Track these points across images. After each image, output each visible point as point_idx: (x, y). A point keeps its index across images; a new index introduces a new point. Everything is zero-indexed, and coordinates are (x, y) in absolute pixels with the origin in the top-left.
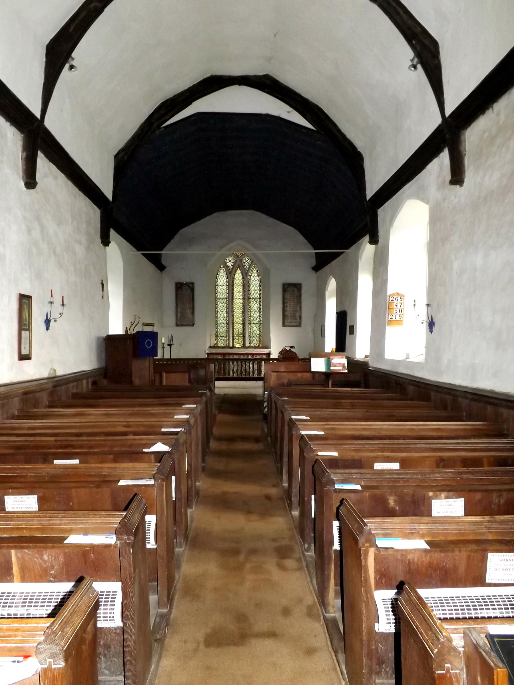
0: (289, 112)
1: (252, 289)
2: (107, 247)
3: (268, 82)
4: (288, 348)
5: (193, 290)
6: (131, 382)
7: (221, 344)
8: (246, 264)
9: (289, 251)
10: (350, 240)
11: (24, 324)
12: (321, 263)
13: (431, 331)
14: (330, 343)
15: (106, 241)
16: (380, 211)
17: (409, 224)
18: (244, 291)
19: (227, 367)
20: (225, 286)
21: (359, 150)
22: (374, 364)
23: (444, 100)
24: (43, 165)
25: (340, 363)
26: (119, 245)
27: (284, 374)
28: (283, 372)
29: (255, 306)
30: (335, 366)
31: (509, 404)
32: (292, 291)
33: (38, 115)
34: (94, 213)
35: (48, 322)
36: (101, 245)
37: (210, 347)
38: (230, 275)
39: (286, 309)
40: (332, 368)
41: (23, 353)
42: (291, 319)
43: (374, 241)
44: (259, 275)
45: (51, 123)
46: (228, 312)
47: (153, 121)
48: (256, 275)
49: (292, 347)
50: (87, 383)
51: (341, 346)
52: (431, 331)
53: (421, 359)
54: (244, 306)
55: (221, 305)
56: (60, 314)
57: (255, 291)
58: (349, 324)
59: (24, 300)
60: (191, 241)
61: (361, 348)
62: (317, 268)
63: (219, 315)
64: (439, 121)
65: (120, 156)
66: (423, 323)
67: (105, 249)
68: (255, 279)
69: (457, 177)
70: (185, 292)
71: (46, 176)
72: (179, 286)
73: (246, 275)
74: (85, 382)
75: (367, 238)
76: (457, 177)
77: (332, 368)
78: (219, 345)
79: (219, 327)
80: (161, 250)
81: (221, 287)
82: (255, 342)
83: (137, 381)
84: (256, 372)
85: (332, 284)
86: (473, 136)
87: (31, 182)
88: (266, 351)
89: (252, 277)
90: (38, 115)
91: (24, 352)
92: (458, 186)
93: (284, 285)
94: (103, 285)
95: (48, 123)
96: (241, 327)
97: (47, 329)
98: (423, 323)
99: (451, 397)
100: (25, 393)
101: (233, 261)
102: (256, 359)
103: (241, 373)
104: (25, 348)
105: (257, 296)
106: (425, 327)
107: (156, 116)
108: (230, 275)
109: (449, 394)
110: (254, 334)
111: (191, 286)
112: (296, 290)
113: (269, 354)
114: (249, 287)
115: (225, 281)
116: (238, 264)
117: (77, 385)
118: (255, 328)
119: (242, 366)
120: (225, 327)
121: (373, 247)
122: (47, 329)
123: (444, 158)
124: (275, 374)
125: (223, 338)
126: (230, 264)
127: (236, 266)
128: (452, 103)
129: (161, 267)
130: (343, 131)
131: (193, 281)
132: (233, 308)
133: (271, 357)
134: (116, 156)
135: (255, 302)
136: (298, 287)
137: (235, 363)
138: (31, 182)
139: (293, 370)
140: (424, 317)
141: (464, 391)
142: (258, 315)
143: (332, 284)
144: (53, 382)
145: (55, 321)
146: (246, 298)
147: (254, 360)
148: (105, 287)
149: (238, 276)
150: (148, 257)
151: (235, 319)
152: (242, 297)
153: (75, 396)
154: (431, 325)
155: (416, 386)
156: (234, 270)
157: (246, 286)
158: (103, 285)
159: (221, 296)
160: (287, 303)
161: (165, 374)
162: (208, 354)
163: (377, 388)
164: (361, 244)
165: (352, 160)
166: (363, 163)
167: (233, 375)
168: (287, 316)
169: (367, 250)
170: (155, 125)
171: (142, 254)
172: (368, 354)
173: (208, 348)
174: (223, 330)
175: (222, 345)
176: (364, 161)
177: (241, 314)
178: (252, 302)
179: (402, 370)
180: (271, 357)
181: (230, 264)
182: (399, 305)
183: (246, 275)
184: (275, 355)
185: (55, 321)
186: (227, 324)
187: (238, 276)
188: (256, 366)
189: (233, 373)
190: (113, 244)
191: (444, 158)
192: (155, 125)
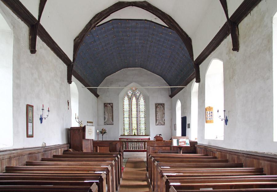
0: (156, 19)
1: (141, 107)
2: (70, 84)
3: (146, 4)
4: (158, 135)
5: (112, 107)
6: (82, 151)
7: (126, 134)
8: (138, 94)
9: (158, 89)
10: (186, 82)
11: (29, 120)
12: (173, 94)
13: (226, 124)
14: (179, 132)
15: (70, 81)
16: (200, 66)
17: (214, 70)
18: (137, 107)
19: (129, 145)
20: (128, 105)
21: (190, 36)
22: (200, 142)
23: (227, 10)
24: (39, 42)
25: (183, 141)
26: (76, 84)
27: (156, 147)
28: (156, 147)
29: (142, 115)
30: (181, 143)
31: (265, 158)
32: (159, 106)
33: (37, 19)
34: (64, 67)
35: (41, 119)
36: (68, 83)
37: (121, 135)
38: (130, 99)
39: (157, 118)
40: (179, 144)
41: (31, 124)
42: (160, 122)
43: (198, 81)
44: (144, 100)
45: (43, 22)
46: (129, 118)
47: (92, 23)
48: (143, 99)
49: (160, 135)
50: (61, 150)
51: (184, 134)
52: (226, 124)
53: (222, 139)
54: (137, 115)
55: (126, 114)
56: (47, 116)
57: (142, 108)
58: (187, 123)
59: (29, 108)
60: (111, 83)
61: (193, 135)
62: (171, 96)
63: (125, 120)
64: (225, 20)
65: (77, 40)
66: (222, 120)
67: (70, 86)
68: (142, 101)
69: (236, 47)
70: (109, 108)
71: (41, 48)
72: (105, 105)
73: (137, 99)
74: (60, 149)
75: (195, 80)
76: (236, 47)
77: (179, 144)
78: (125, 134)
79: (125, 126)
80: (98, 87)
81: (126, 106)
82: (143, 132)
83: (85, 151)
84: (143, 148)
85: (179, 104)
86: (243, 26)
87: (33, 50)
88: (147, 137)
89: (141, 100)
90: (37, 19)
91: (30, 133)
92: (236, 51)
93: (156, 104)
94: (68, 103)
95: (42, 22)
96: (136, 126)
97: (41, 122)
98: (222, 120)
99: (237, 156)
100: (30, 154)
101: (131, 92)
102: (143, 141)
103: (136, 148)
104: (30, 131)
105: (143, 110)
106: (223, 122)
107: (93, 21)
108: (130, 99)
109: (235, 155)
110: (142, 129)
111: (111, 105)
112: (162, 107)
113: (149, 139)
114: (139, 105)
115: (128, 103)
116: (134, 94)
117: (56, 151)
118: (142, 126)
119: (136, 145)
120: (128, 126)
121: (198, 84)
122: (41, 122)
123: (229, 38)
124: (152, 147)
125: (127, 131)
126: (130, 94)
127: (133, 95)
128: (232, 11)
129: (97, 96)
130: (181, 27)
131: (112, 103)
132: (132, 116)
133: (150, 140)
134: (75, 40)
135: (142, 113)
136: (163, 105)
137: (133, 143)
138: (33, 50)
139: (161, 146)
140: (223, 117)
141: (243, 153)
142: (144, 119)
143: (179, 104)
144: (44, 149)
145: (45, 119)
146: (138, 111)
147: (142, 142)
148: (69, 103)
149: (134, 100)
150: (91, 90)
151: (133, 121)
152: (136, 123)
153: (54, 156)
154: (226, 121)
155: (220, 152)
156: (132, 97)
157: (138, 105)
158: (68, 103)
159: (126, 110)
160: (158, 111)
161: (98, 147)
162: (120, 139)
163: (201, 154)
164: (192, 83)
165: (187, 41)
166: (192, 43)
167: (132, 149)
168: (158, 111)
169: (195, 86)
170: (93, 25)
171: (88, 88)
172: (197, 137)
173: (120, 136)
174: (127, 127)
175: (127, 134)
176: (192, 42)
177: (136, 119)
178: (141, 113)
179: (213, 144)
180: (150, 140)
181: (130, 94)
182: (211, 118)
183: (137, 99)
184: (152, 138)
185: (45, 119)
186: (129, 124)
187: (134, 100)
188: (143, 145)
189: (132, 148)
190: (73, 83)
191: (229, 38)
192: (93, 25)
